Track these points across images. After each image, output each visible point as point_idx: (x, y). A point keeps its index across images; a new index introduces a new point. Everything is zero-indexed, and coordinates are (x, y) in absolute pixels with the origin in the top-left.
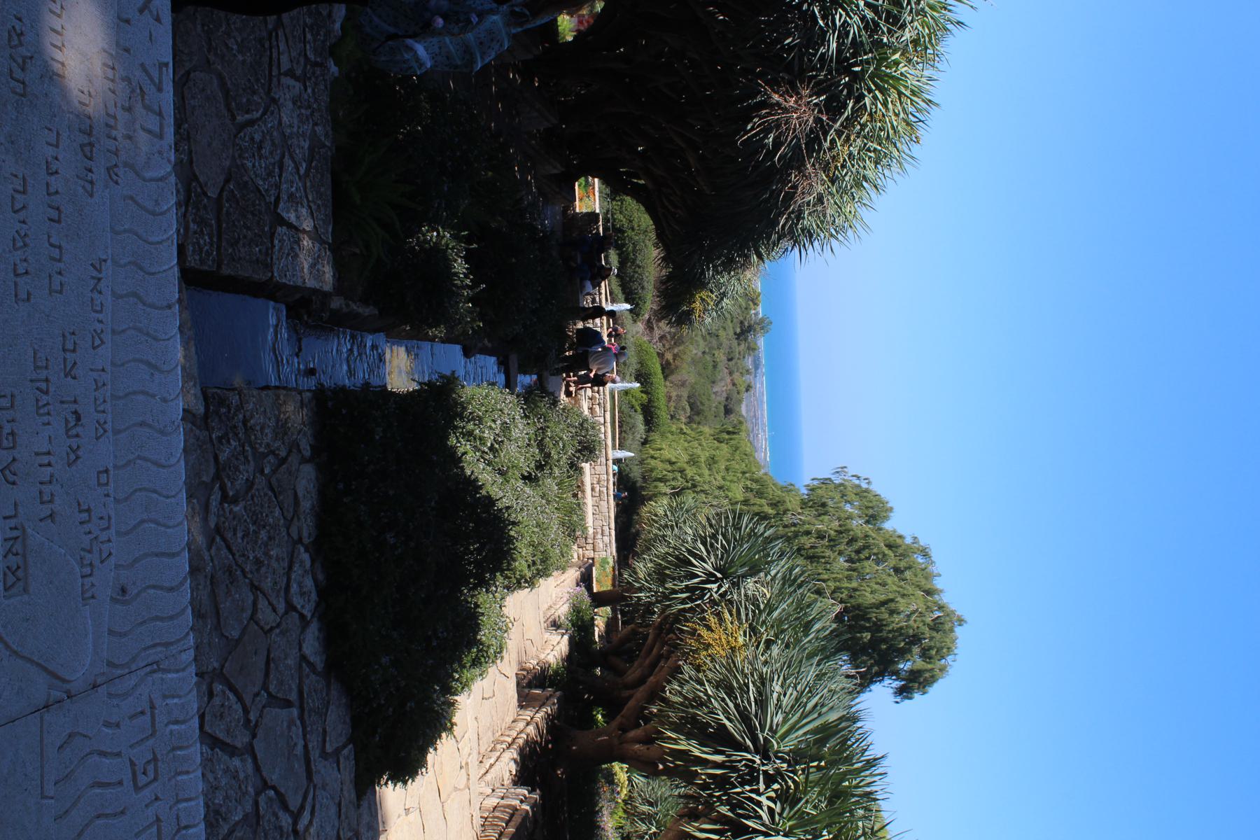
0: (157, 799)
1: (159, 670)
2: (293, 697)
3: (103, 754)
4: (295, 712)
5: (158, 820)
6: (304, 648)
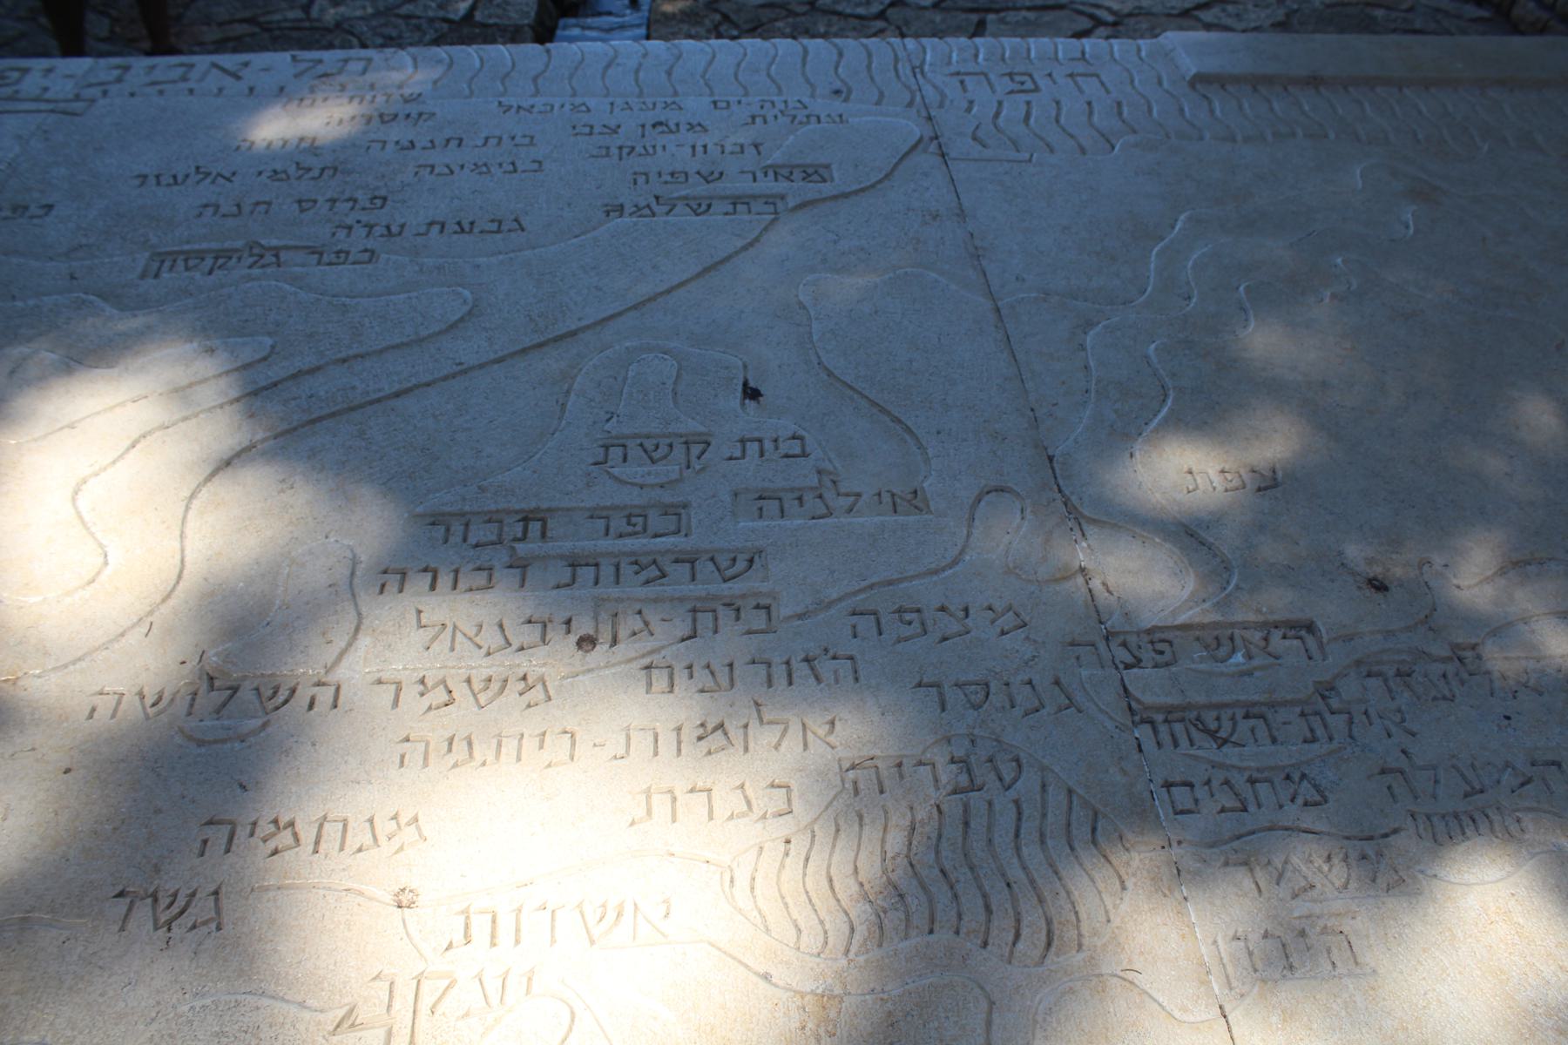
0: (1050, 75)
1: (921, 67)
2: (975, 17)
3: (997, 115)
4: (991, 17)
5: (1071, 75)
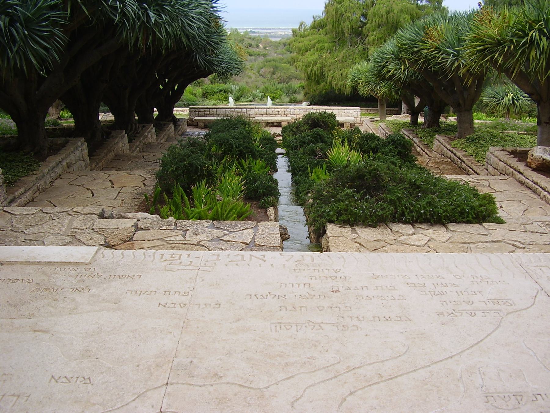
6: (444, 241)
